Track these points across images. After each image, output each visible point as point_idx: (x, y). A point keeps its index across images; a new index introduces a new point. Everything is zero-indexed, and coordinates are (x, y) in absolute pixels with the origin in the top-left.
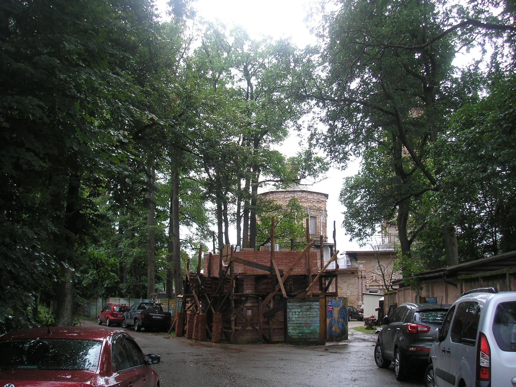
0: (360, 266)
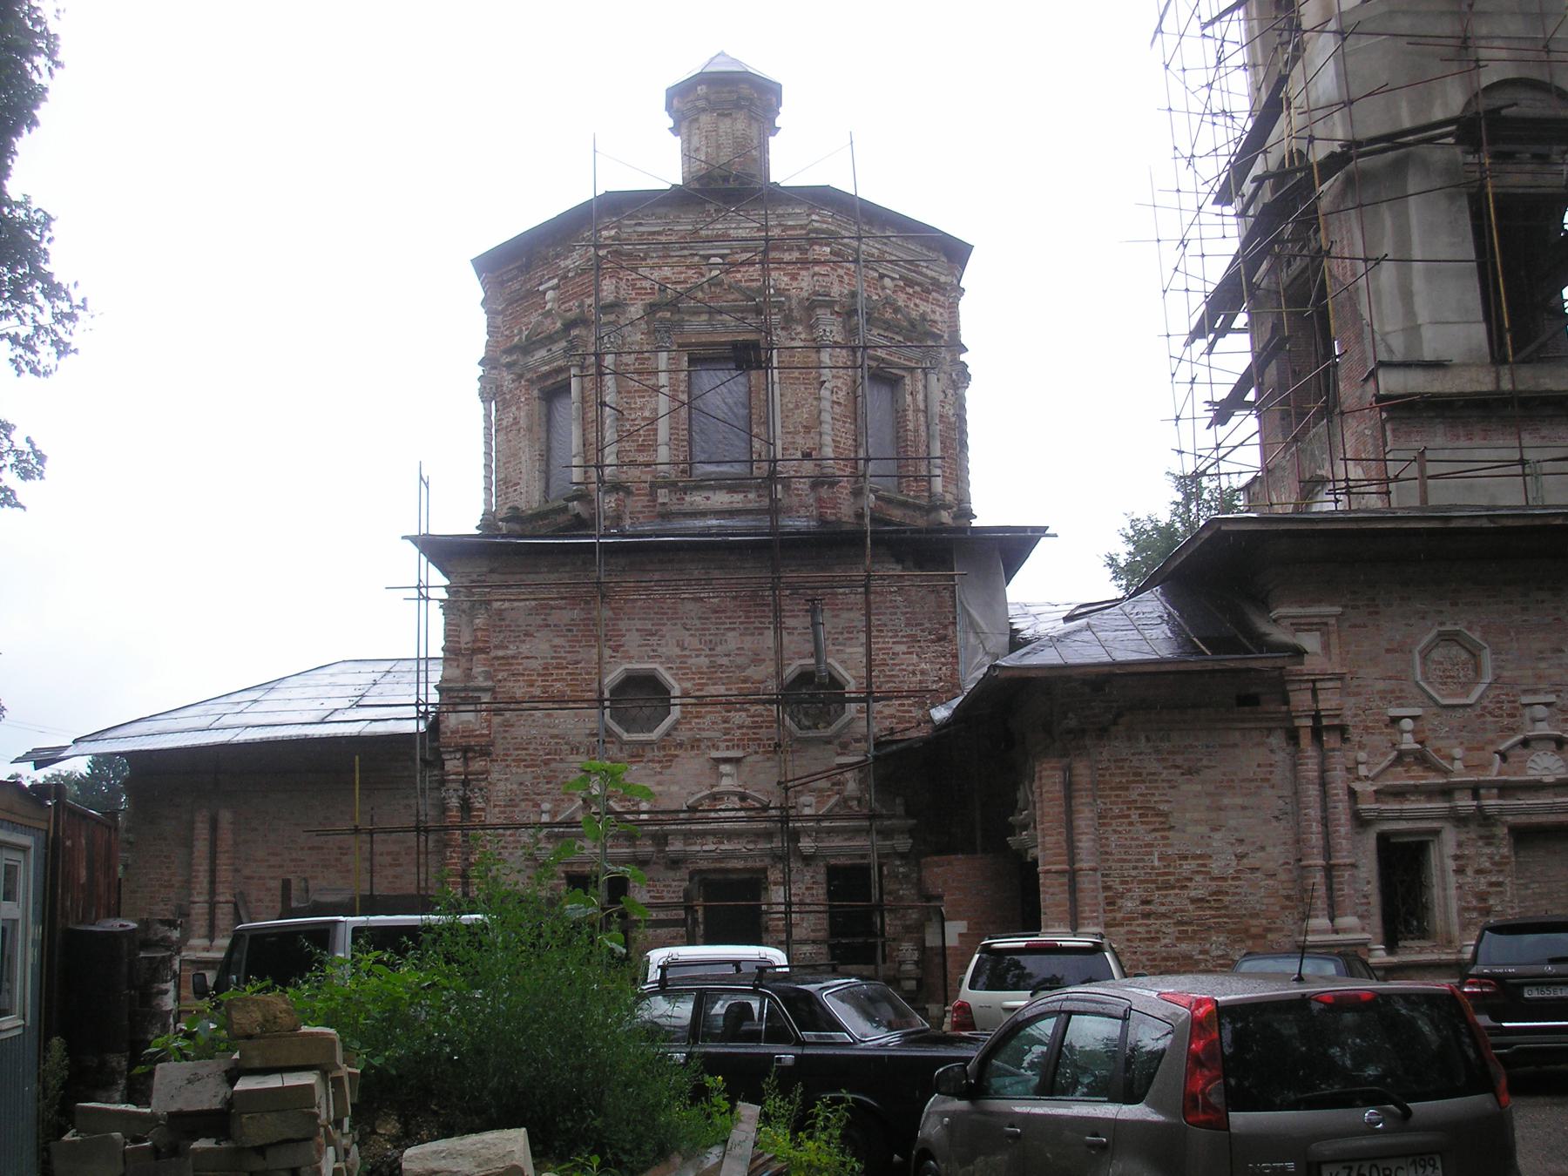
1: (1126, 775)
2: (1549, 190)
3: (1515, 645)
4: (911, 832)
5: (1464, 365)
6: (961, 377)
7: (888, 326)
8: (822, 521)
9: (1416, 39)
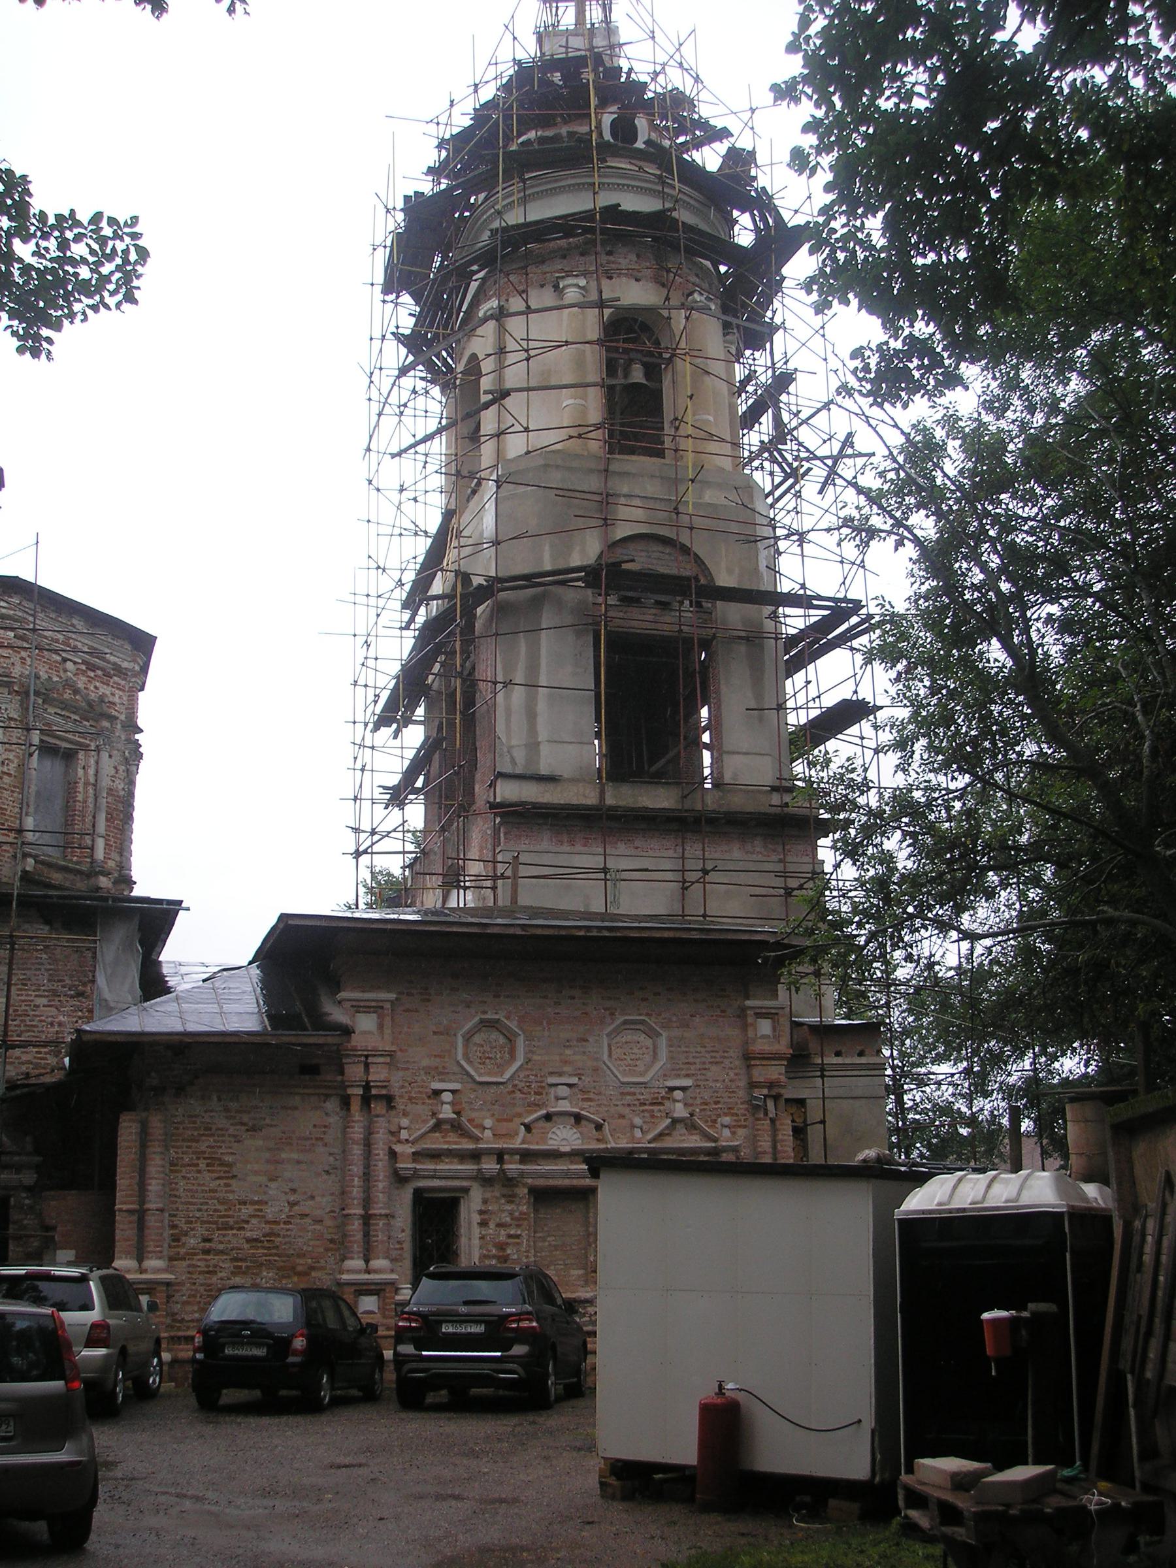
0: (363, 1019)
1: (196, 1129)
2: (666, 633)
3: (546, 1033)
5: (574, 780)
6: (134, 755)
7: (65, 705)
9: (565, 493)
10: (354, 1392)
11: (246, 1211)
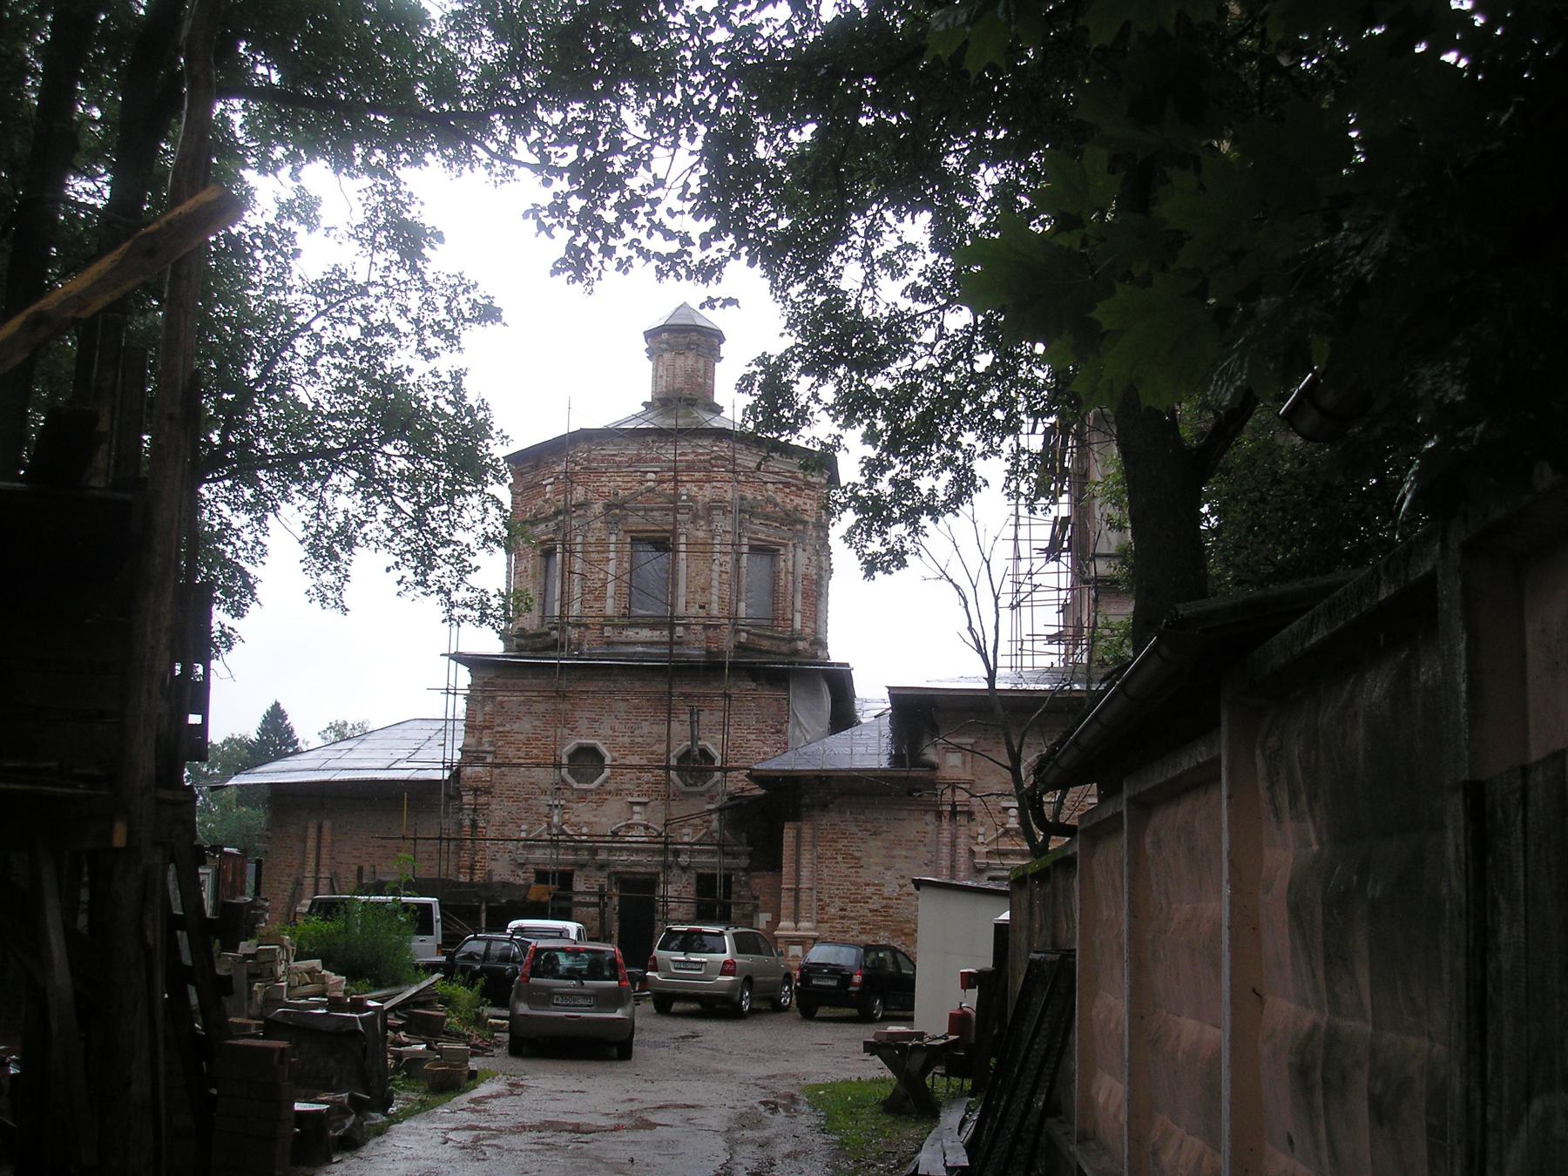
4: (750, 855)
8: (709, 652)
10: (764, 1006)
11: (870, 890)
